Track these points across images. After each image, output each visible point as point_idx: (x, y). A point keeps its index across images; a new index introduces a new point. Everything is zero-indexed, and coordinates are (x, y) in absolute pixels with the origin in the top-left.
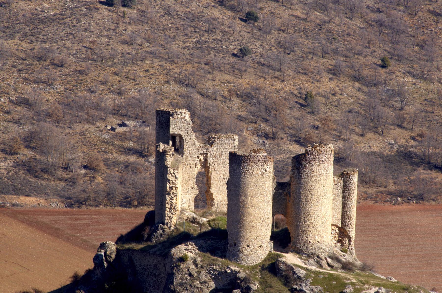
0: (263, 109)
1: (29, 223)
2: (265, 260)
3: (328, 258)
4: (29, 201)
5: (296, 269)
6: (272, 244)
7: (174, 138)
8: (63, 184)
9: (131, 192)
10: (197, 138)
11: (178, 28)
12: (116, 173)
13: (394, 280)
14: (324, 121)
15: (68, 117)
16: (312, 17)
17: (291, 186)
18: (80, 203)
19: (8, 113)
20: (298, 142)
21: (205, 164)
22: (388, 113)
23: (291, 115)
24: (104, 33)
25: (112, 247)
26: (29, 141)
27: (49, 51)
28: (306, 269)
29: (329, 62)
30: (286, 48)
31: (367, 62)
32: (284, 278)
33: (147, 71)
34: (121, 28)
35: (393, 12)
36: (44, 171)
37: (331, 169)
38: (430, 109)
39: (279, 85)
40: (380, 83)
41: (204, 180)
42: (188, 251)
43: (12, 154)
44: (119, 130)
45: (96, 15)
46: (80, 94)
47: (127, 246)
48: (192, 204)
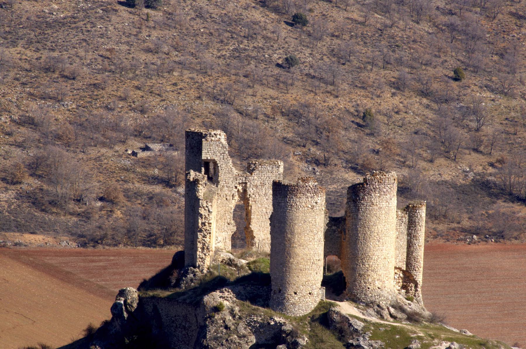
0: (313, 129)
1: (35, 266)
2: (316, 310)
3: (390, 308)
4: (35, 240)
5: (352, 321)
6: (323, 291)
7: (207, 164)
8: (75, 219)
9: (156, 229)
10: (234, 164)
11: (211, 34)
12: (138, 206)
13: (469, 334)
14: (386, 144)
15: (81, 140)
16: (372, 21)
17: (347, 222)
18: (96, 242)
19: (9, 134)
20: (354, 169)
21: (244, 196)
23: (347, 137)
24: (124, 39)
25: (134, 294)
26: (35, 168)
27: (58, 60)
28: (365, 321)
29: (392, 74)
30: (341, 57)
31: (436, 74)
33: (175, 84)
34: (144, 34)
35: (467, 14)
36: (53, 203)
37: (394, 201)
38: (512, 130)
39: (331, 101)
40: (453, 99)
41: (243, 214)
42: (224, 299)
44: (142, 155)
45: (114, 18)
46: (95, 112)
47: (151, 293)
48: (229, 243)
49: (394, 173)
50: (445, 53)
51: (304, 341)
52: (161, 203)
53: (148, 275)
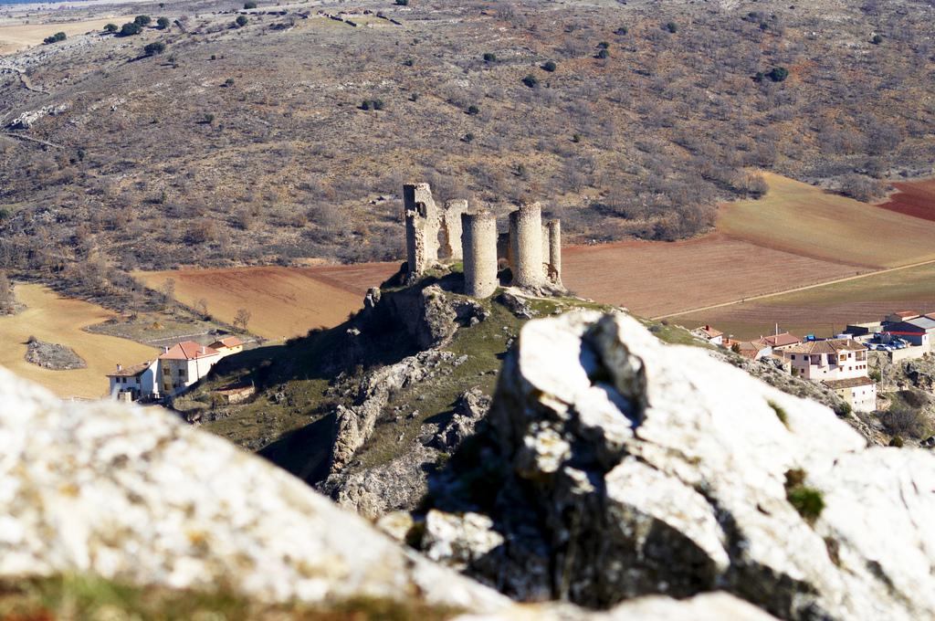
0: (487, 179)
1: (316, 278)
2: (494, 294)
4: (314, 262)
7: (418, 205)
8: (339, 247)
9: (391, 250)
11: (418, 123)
12: (378, 236)
13: (592, 301)
14: (534, 186)
15: (339, 196)
16: (520, 108)
18: (353, 260)
19: (295, 196)
20: (515, 203)
21: (444, 224)
22: (582, 176)
23: (509, 183)
24: (362, 130)
25: (377, 291)
26: (312, 216)
27: (322, 147)
28: (526, 298)
29: (535, 141)
30: (501, 132)
31: (563, 138)
32: (559, 426)
33: (397, 157)
34: (375, 126)
35: (579, 100)
36: (325, 238)
37: (540, 220)
39: (497, 161)
41: (444, 236)
42: (434, 291)
43: (298, 227)
44: (378, 203)
46: (347, 178)
48: (436, 255)
49: (538, 203)
50: (568, 125)
51: (488, 314)
52: (393, 233)
53: (385, 280)
